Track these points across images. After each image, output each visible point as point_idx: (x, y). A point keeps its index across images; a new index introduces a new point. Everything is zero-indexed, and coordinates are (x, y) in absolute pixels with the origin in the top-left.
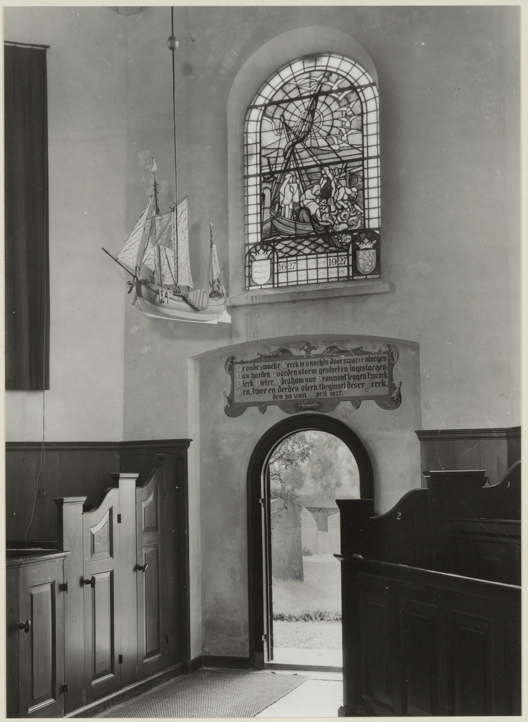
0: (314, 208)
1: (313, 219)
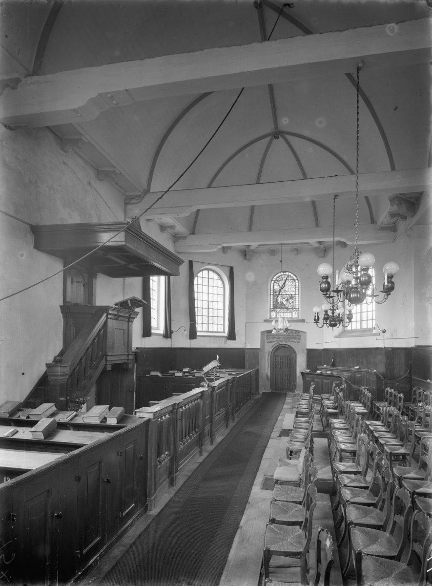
0: (285, 303)
1: (284, 305)
